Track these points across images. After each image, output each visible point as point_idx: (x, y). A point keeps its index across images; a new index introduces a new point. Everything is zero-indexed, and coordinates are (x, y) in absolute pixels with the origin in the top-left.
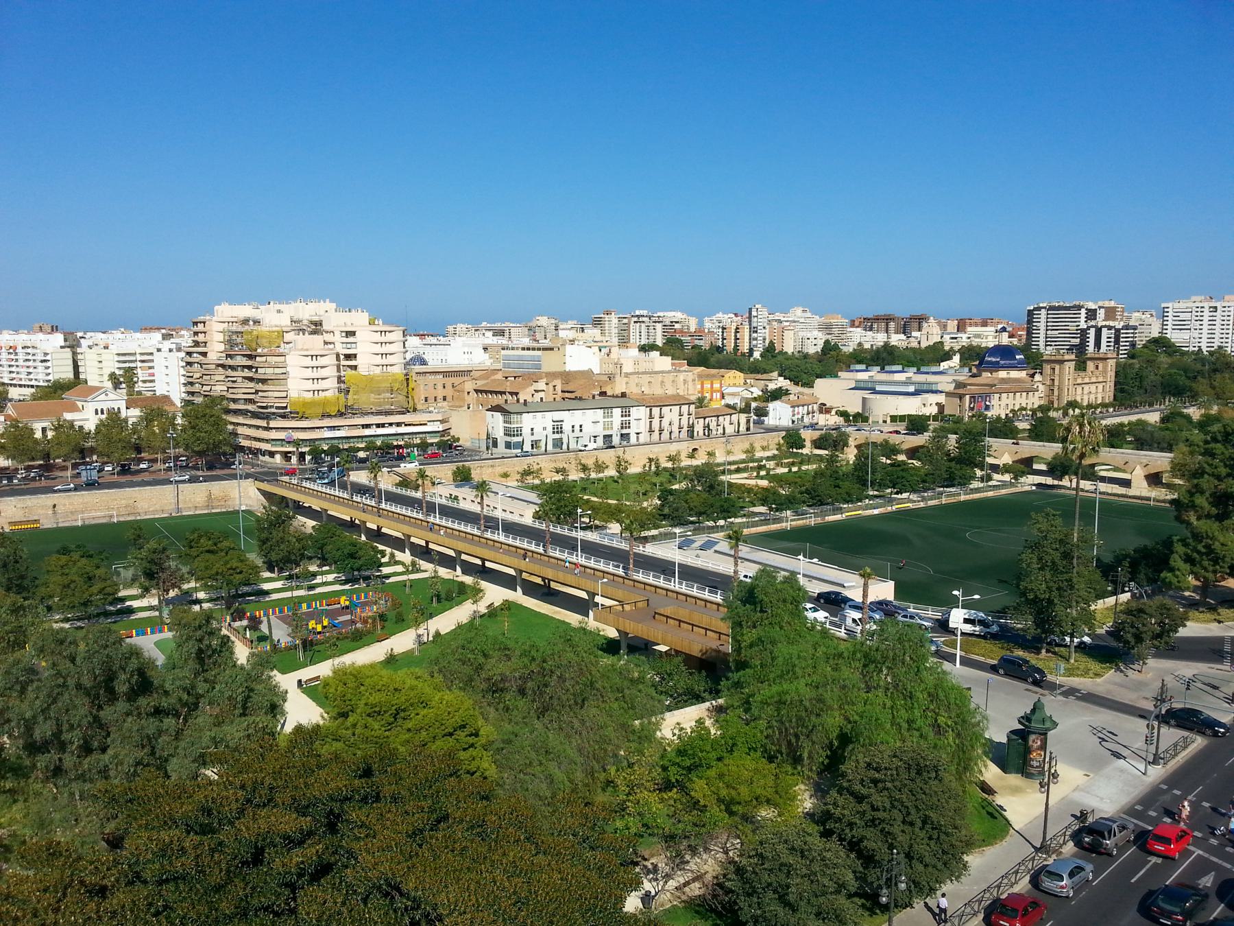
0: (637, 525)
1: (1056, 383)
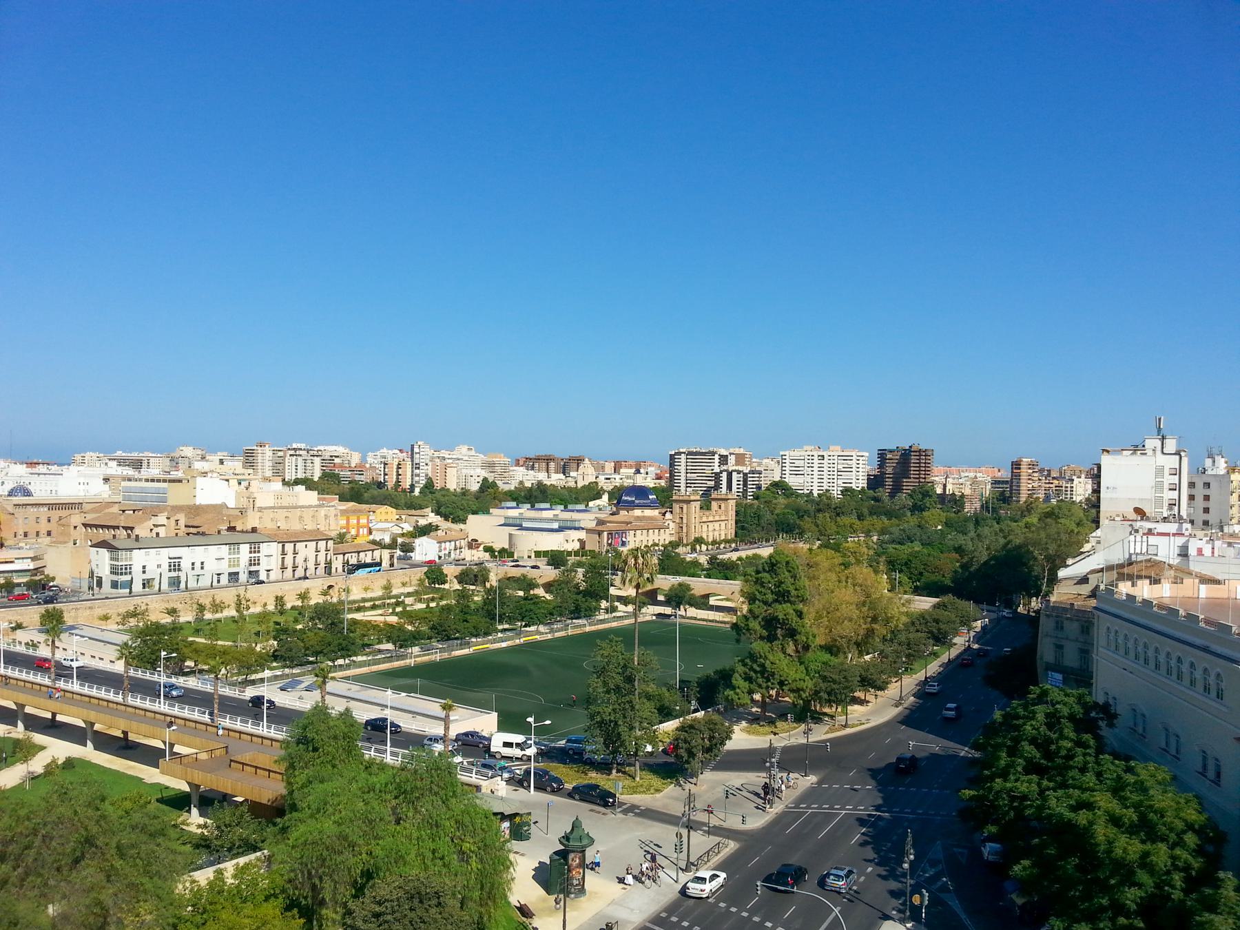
0: (248, 665)
1: (685, 521)
